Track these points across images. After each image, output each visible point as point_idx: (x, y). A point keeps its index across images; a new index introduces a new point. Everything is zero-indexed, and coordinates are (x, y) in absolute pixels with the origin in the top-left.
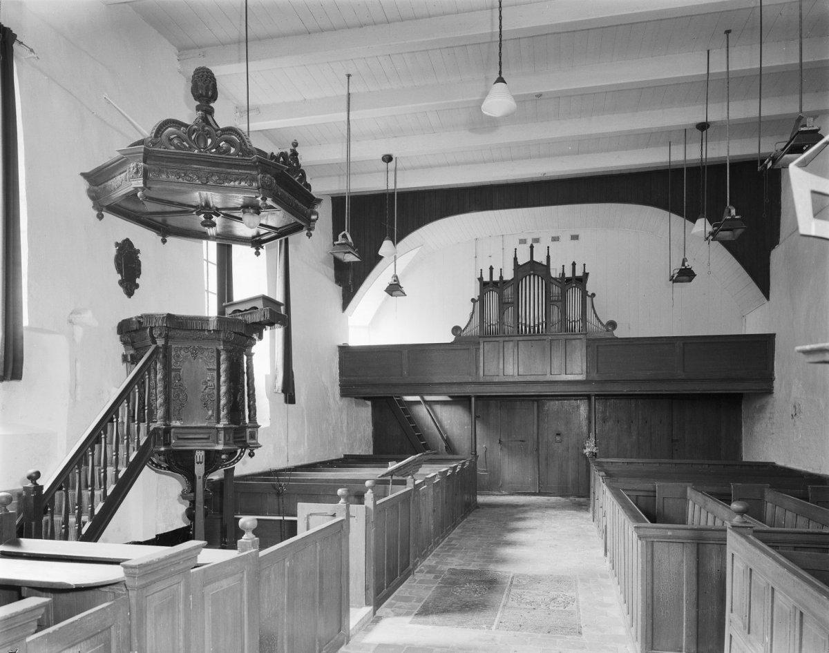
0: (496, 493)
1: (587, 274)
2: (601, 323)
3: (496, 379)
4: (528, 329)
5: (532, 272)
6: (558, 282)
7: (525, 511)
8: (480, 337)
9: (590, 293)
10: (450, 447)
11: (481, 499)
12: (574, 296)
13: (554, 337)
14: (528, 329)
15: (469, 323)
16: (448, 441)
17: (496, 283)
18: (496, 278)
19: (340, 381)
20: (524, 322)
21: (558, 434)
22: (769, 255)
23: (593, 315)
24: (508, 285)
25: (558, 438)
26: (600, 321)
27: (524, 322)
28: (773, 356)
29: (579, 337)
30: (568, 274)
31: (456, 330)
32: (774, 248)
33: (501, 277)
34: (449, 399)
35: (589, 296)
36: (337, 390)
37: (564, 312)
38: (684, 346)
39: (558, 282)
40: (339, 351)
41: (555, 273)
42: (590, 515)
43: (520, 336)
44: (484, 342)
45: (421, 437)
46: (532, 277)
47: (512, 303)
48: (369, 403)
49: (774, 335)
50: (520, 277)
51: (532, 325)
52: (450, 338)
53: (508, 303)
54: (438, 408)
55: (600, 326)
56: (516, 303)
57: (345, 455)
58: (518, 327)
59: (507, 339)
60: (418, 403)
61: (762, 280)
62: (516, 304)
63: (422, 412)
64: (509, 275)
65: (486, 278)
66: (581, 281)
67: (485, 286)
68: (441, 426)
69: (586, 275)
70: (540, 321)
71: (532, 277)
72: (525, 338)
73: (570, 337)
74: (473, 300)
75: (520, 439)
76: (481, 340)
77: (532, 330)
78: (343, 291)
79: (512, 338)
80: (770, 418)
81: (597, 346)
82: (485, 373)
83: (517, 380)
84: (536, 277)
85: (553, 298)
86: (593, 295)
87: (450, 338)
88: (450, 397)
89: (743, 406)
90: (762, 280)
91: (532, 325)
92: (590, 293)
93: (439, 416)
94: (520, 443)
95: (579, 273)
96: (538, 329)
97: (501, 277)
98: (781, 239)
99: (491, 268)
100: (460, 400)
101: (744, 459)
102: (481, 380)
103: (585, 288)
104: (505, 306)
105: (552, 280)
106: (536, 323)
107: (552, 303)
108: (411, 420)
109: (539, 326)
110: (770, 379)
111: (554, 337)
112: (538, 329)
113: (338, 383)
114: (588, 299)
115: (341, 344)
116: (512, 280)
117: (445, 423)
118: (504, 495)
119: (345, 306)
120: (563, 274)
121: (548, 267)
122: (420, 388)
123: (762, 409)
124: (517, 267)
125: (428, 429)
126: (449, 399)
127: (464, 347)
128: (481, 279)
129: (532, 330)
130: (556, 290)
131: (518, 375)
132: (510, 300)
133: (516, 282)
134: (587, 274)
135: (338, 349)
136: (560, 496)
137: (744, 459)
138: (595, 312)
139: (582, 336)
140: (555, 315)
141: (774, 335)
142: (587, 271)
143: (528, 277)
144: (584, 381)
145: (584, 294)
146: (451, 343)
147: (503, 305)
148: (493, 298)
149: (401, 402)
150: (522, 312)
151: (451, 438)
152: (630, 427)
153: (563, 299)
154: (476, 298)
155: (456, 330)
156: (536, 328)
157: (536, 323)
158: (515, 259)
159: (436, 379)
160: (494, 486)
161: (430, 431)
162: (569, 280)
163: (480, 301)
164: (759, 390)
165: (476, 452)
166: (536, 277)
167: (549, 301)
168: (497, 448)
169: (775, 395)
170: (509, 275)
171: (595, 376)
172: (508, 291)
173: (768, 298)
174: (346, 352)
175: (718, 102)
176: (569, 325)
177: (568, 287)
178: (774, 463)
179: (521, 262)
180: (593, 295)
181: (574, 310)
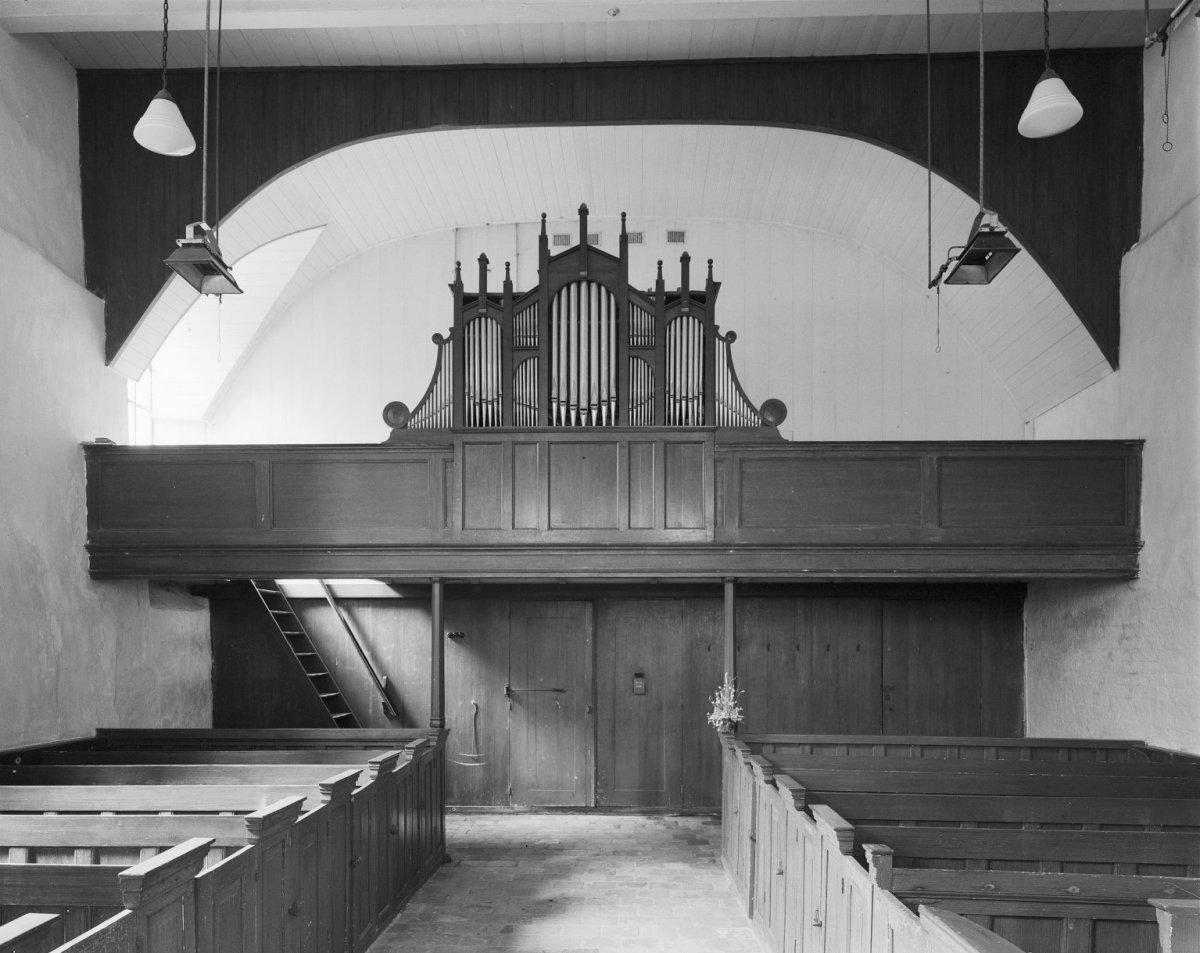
0: (499, 808)
1: (718, 285)
2: (750, 405)
3: (494, 538)
4: (573, 414)
5: (583, 274)
6: (651, 303)
7: (564, 871)
8: (453, 431)
9: (723, 332)
10: (396, 707)
11: (459, 827)
12: (685, 335)
13: (637, 437)
14: (573, 414)
15: (426, 397)
16: (389, 691)
17: (494, 299)
18: (495, 286)
19: (89, 536)
20: (563, 397)
21: (639, 675)
22: (1118, 264)
23: (732, 386)
24: (524, 304)
25: (639, 684)
26: (746, 400)
27: (563, 397)
28: (1138, 493)
29: (696, 436)
30: (672, 284)
31: (394, 412)
32: (1128, 249)
33: (508, 284)
34: (392, 593)
35: (721, 338)
36: (81, 561)
37: (660, 375)
38: (940, 465)
39: (651, 303)
40: (88, 458)
41: (641, 278)
42: (724, 880)
43: (554, 431)
44: (465, 443)
45: (325, 683)
46: (584, 286)
47: (536, 349)
48: (206, 602)
49: (1141, 443)
50: (554, 286)
51: (584, 404)
52: (381, 433)
53: (527, 349)
54: (366, 615)
55: (747, 411)
56: (543, 347)
57: (99, 731)
58: (550, 411)
59: (521, 437)
60: (320, 602)
61: (1104, 324)
62: (544, 353)
63: (329, 624)
64: (527, 279)
65: (471, 286)
66: (702, 303)
67: (467, 305)
68: (375, 656)
69: (713, 287)
70: (604, 396)
71: (584, 286)
72: (566, 437)
73: (672, 436)
74: (437, 338)
75: (553, 686)
76: (458, 440)
77: (583, 418)
78: (107, 308)
79: (536, 437)
80: (1122, 638)
81: (742, 461)
82: (469, 523)
83: (546, 541)
84: (594, 287)
85: (637, 341)
86: (732, 336)
87: (381, 433)
88: (393, 584)
89: (1025, 616)
90: (1104, 324)
91: (584, 404)
92: (723, 332)
93: (371, 634)
94: (554, 695)
95: (698, 284)
96: (599, 417)
97: (508, 284)
98: (1144, 232)
99: (483, 261)
100: (411, 595)
101: (1029, 734)
102: (458, 538)
103: (713, 319)
104: (518, 356)
105: (635, 298)
106: (594, 400)
107: (633, 353)
108: (302, 641)
109: (600, 411)
110: (1134, 545)
111: (637, 437)
112: (599, 417)
113: (84, 541)
114: (720, 346)
115: (91, 438)
116: (535, 290)
117: (385, 649)
118: (517, 813)
119: (111, 349)
120: (660, 282)
121: (621, 264)
122: (306, 558)
123: (1092, 617)
124: (547, 262)
125: (344, 663)
126: (392, 593)
127: (415, 456)
128: (457, 287)
129: (583, 418)
130: (641, 320)
131: (549, 528)
132: (530, 342)
133: (544, 297)
134: (718, 285)
135: (83, 453)
136: (644, 813)
137: (1029, 734)
138: (734, 378)
139: (702, 436)
140: (641, 385)
141: (1141, 443)
142: (715, 279)
143: (573, 287)
144: (707, 545)
145: (710, 332)
146: (382, 444)
147: (512, 353)
148: (487, 336)
149: (278, 599)
150: (559, 372)
151: (393, 682)
152: (794, 660)
153: (657, 352)
154: (446, 334)
155: (394, 412)
156: (594, 413)
157: (594, 400)
158: (543, 239)
159: (343, 537)
160: (494, 791)
161: (347, 667)
162: (672, 299)
163: (457, 344)
164: (1107, 571)
165: (442, 719)
166: (594, 287)
167: (625, 349)
168: (503, 705)
169: (1137, 585)
170: (527, 279)
171: (733, 532)
172: (526, 320)
173: (1114, 360)
174: (102, 458)
175: (509, 832)
176: (675, 409)
177: (670, 314)
178: (1142, 743)
179: (555, 250)
180: (732, 336)
181: (686, 376)
